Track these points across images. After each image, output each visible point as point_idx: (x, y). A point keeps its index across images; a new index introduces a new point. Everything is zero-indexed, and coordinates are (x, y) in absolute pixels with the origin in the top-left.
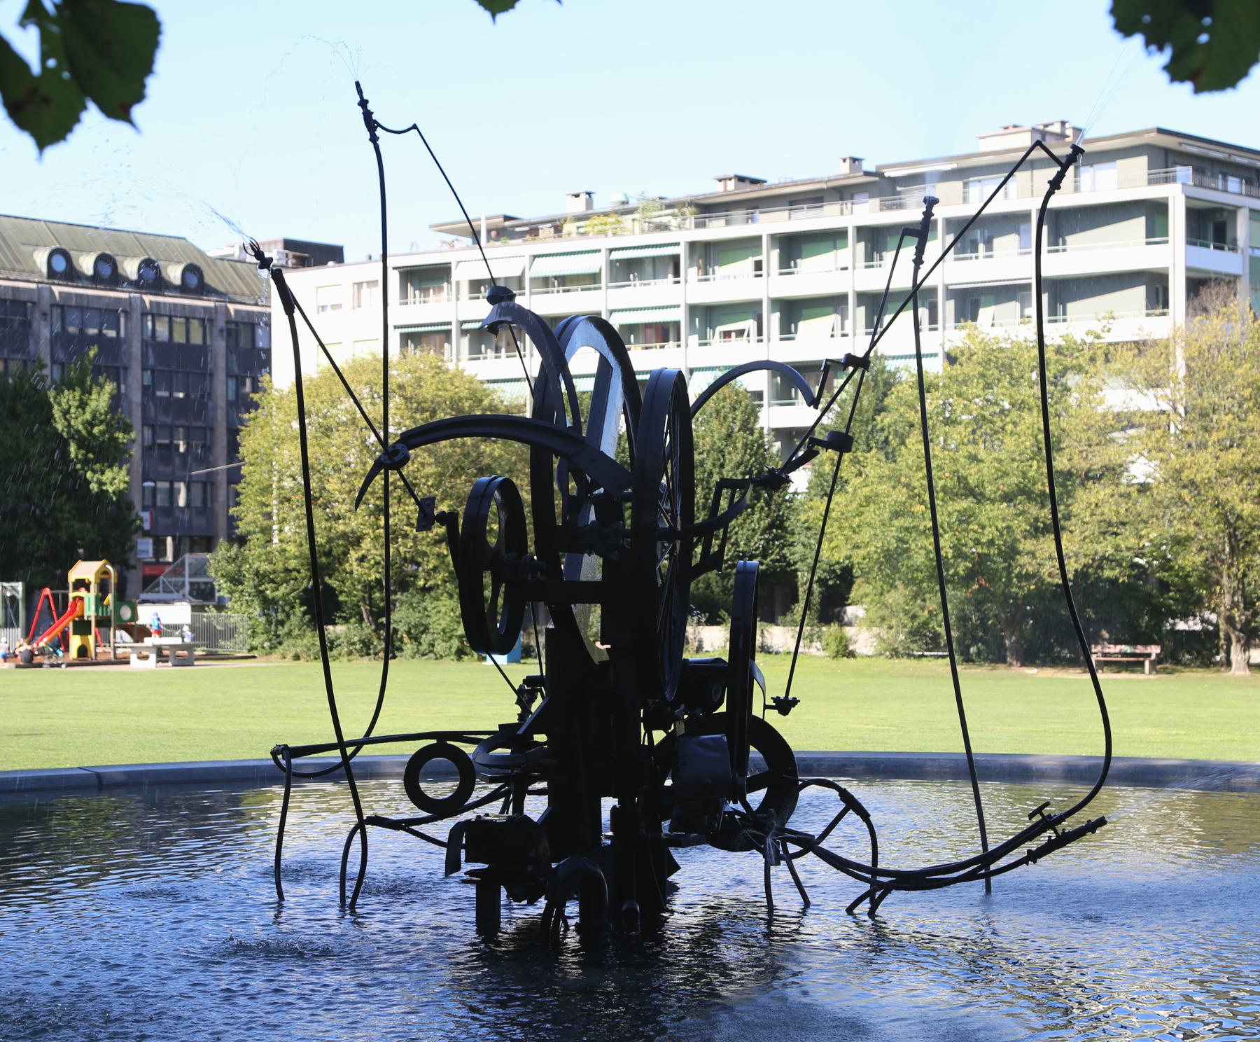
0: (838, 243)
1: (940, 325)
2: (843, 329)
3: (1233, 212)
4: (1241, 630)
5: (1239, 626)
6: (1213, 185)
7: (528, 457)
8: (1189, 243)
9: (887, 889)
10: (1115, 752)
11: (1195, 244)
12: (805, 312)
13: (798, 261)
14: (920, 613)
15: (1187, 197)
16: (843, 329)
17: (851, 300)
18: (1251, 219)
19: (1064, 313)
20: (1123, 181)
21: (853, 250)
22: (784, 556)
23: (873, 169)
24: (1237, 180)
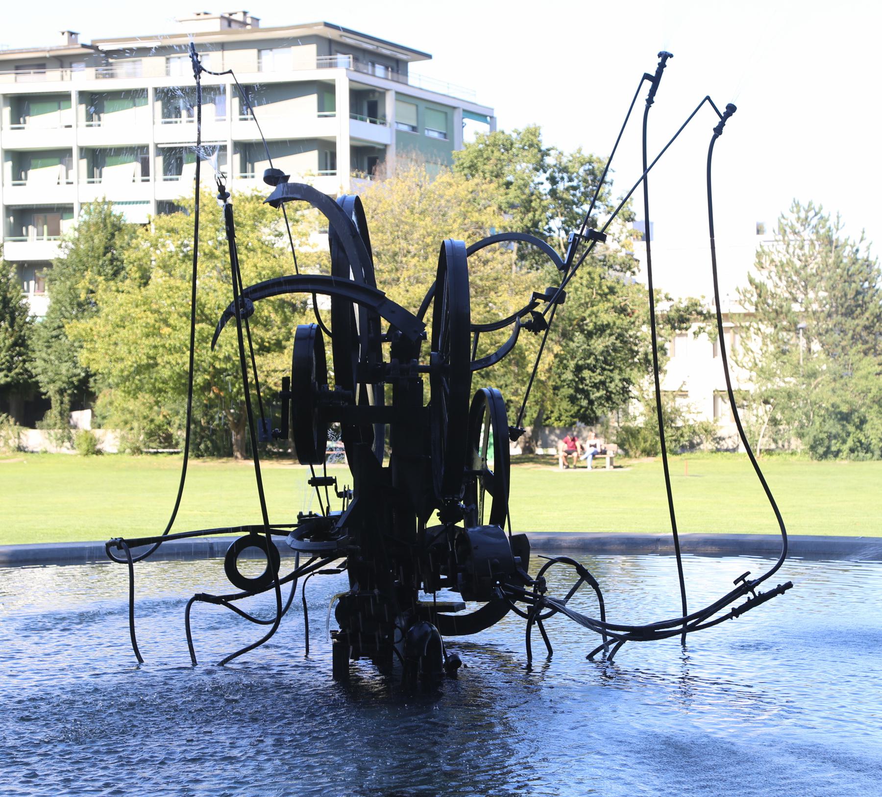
0: (62, 104)
1: (151, 177)
2: (67, 178)
3: (383, 93)
6: (365, 71)
8: (351, 117)
9: (622, 640)
10: (788, 533)
11: (356, 118)
12: (33, 162)
13: (27, 118)
14: (156, 418)
15: (350, 80)
16: (67, 178)
17: (75, 153)
18: (397, 100)
19: (253, 171)
20: (300, 64)
21: (76, 111)
22: (26, 370)
23: (89, 43)
24: (382, 67)
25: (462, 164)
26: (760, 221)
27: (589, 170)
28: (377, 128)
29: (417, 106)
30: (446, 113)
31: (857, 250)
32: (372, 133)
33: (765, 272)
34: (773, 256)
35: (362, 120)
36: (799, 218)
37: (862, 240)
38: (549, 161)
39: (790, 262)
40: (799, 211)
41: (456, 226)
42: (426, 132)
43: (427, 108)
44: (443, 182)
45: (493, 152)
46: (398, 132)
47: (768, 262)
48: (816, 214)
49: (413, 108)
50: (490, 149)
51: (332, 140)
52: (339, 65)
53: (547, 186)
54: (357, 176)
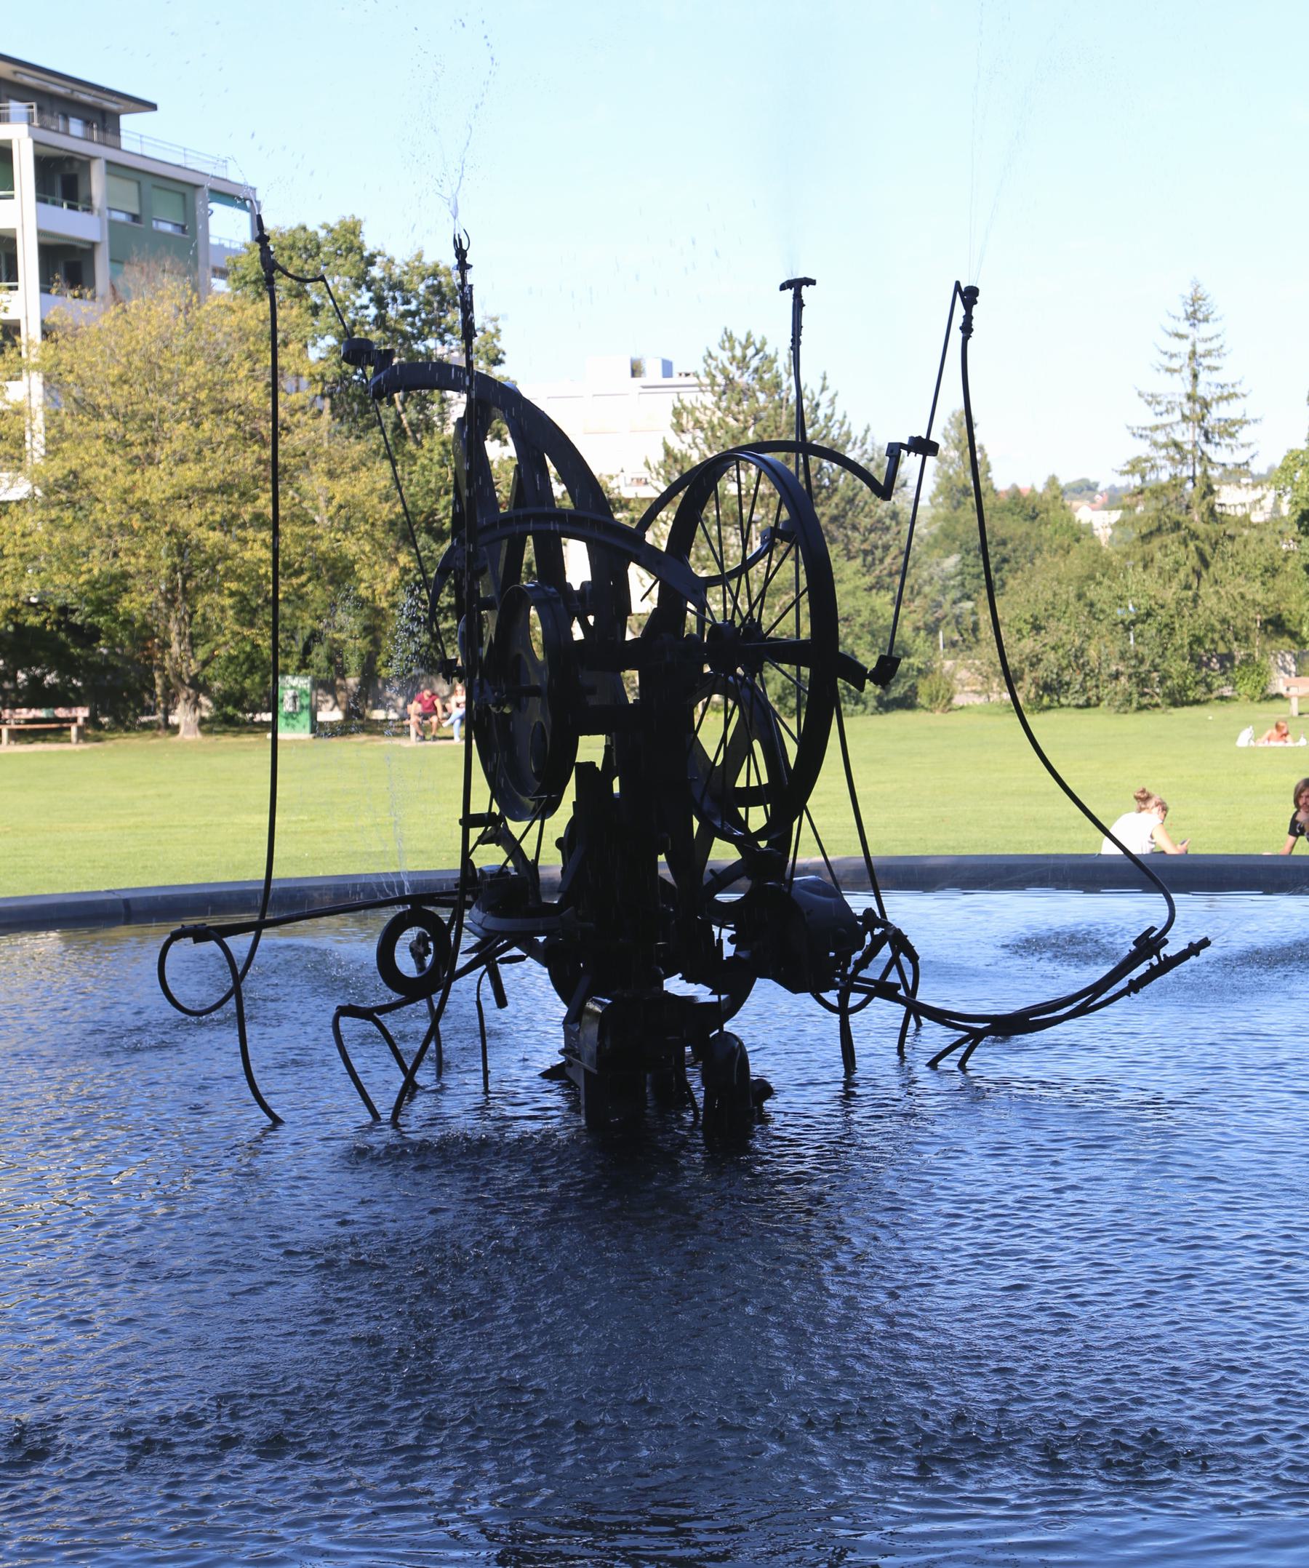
3: (85, 163)
4: (191, 686)
5: (187, 681)
7: (843, 630)
8: (40, 199)
15: (36, 142)
18: (108, 173)
24: (80, 122)
25: (244, 277)
26: (636, 356)
27: (433, 286)
28: (79, 216)
29: (139, 183)
30: (184, 195)
31: (818, 405)
32: (75, 225)
33: (687, 438)
34: (697, 414)
35: (54, 203)
36: (734, 357)
37: (823, 389)
38: (376, 272)
39: (723, 423)
40: (732, 349)
41: (242, 373)
42: (154, 223)
43: (154, 186)
44: (219, 306)
45: (291, 258)
46: (113, 224)
47: (691, 424)
48: (757, 353)
49: (134, 187)
50: (286, 253)
51: (11, 235)
52: (11, 117)
53: (372, 311)
54: (80, 296)
